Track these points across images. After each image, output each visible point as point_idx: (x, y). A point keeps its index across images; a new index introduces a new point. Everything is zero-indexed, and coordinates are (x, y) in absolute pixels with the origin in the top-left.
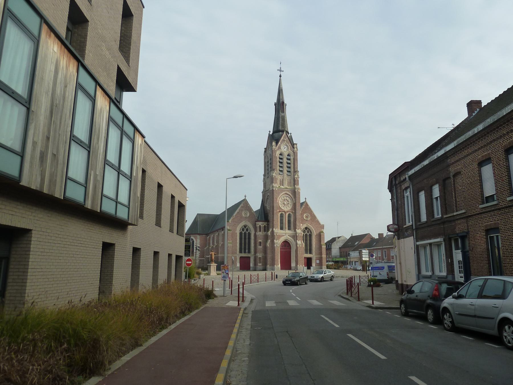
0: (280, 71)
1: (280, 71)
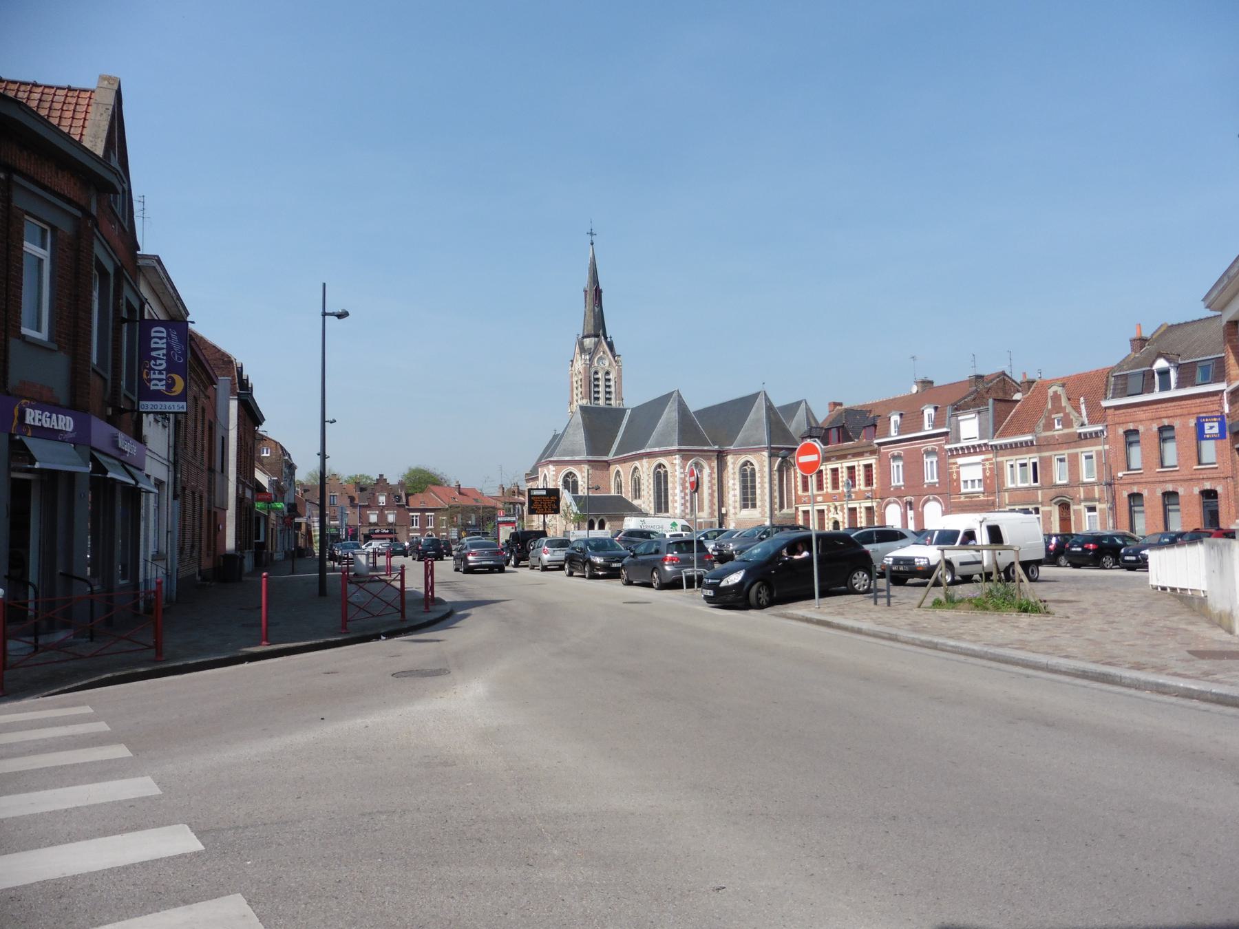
0: (592, 234)
1: (592, 234)
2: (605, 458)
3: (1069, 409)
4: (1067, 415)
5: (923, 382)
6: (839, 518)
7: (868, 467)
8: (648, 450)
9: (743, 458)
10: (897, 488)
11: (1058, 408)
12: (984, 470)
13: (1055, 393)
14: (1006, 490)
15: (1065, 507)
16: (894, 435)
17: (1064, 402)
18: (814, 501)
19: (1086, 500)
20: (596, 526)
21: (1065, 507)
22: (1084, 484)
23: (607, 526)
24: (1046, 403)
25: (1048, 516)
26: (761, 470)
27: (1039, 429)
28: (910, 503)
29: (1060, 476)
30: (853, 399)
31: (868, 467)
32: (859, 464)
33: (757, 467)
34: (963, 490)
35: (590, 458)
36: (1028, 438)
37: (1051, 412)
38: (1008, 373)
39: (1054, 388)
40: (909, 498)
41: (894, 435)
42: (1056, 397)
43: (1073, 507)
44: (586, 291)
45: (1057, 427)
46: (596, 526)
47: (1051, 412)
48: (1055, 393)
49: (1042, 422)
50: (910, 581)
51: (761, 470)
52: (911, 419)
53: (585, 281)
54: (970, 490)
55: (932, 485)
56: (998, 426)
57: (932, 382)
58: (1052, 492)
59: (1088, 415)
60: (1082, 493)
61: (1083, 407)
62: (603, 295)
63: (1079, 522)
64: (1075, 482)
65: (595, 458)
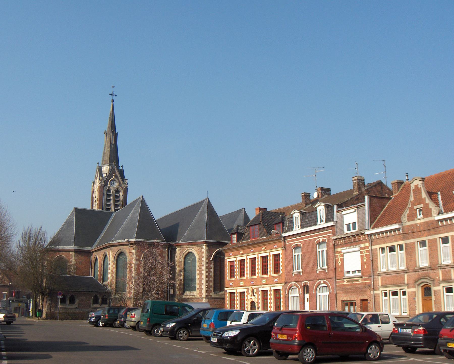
0: (113, 95)
1: (113, 95)
2: (89, 249)
3: (428, 201)
4: (427, 205)
5: (322, 189)
6: (255, 299)
7: (277, 257)
8: (114, 242)
9: (187, 249)
10: (298, 274)
11: (419, 200)
12: (362, 257)
13: (416, 186)
14: (380, 274)
15: (427, 291)
16: (296, 230)
17: (424, 195)
18: (237, 285)
19: (444, 281)
20: (68, 302)
21: (427, 291)
22: (443, 267)
23: (77, 301)
24: (409, 196)
25: (413, 297)
26: (200, 259)
27: (404, 218)
28: (307, 287)
29: (423, 259)
30: (272, 206)
31: (277, 257)
32: (270, 253)
33: (197, 257)
34: (346, 275)
35: (76, 248)
36: (396, 226)
37: (413, 204)
38: (384, 182)
39: (416, 183)
40: (305, 283)
41: (296, 230)
42: (417, 190)
43: (434, 288)
44: (106, 133)
45: (419, 217)
46: (68, 302)
47: (413, 204)
48: (416, 186)
49: (407, 212)
50: (290, 357)
51: (200, 259)
52: (308, 217)
53: (106, 126)
54: (351, 275)
55: (323, 272)
56: (374, 220)
57: (329, 190)
58: (415, 275)
59: (444, 205)
60: (440, 275)
61: (440, 198)
62: (119, 137)
63: (438, 302)
64: (434, 266)
65: (81, 248)
